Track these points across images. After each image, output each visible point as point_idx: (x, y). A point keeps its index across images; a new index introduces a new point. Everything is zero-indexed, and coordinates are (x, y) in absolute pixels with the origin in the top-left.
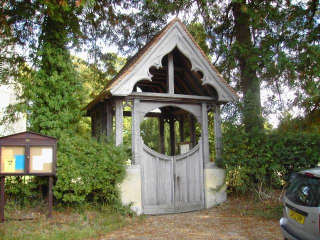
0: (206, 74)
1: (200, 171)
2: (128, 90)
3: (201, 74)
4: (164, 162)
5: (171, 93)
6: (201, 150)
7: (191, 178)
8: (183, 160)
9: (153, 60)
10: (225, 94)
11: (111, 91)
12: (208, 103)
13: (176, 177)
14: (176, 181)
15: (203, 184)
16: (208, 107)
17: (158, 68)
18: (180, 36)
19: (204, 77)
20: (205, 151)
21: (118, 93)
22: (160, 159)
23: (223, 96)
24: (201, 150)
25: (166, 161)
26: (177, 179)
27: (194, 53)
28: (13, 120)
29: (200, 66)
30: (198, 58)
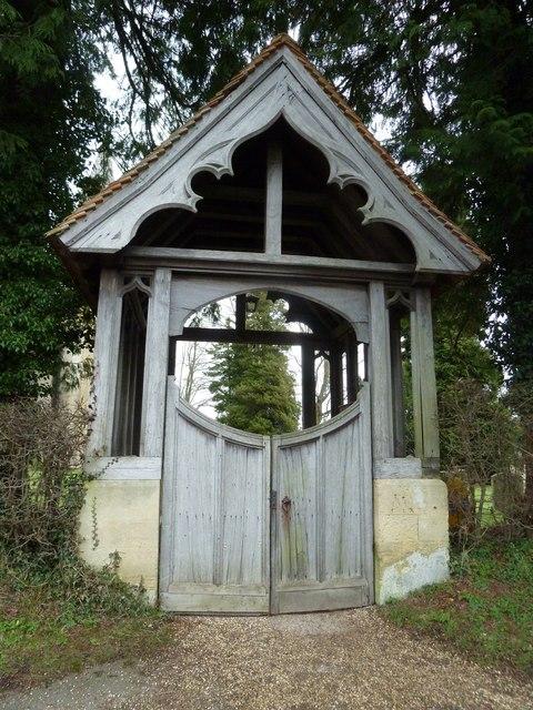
0: (376, 191)
1: (361, 485)
2: (117, 236)
3: (359, 193)
4: (241, 454)
5: (273, 251)
6: (365, 422)
7: (332, 504)
8: (305, 450)
9: (207, 153)
10: (439, 251)
11: (64, 239)
12: (389, 280)
13: (280, 498)
14: (280, 512)
15: (369, 526)
16: (389, 294)
17: (219, 177)
18: (297, 88)
19: (201, 164)
20: (377, 422)
21: (85, 246)
22: (229, 442)
23: (432, 256)
24: (365, 422)
25: (252, 449)
26: (280, 507)
27: (336, 134)
28: (116, 554)
29: (356, 168)
30: (349, 147)
